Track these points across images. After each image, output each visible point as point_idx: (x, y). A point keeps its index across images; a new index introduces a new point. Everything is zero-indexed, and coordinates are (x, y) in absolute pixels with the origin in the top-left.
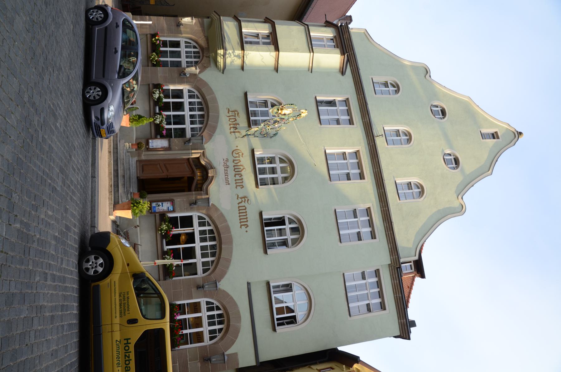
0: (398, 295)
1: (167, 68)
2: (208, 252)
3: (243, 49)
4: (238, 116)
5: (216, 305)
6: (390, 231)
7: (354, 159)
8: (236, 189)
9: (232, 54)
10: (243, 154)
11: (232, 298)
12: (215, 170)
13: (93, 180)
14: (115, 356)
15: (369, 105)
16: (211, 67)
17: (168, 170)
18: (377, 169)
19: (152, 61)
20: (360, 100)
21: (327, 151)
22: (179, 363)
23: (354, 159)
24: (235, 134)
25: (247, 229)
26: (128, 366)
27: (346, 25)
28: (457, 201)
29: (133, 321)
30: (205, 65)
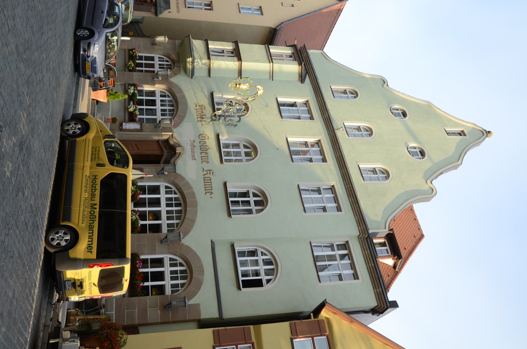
0: (370, 265)
1: (142, 73)
2: (174, 216)
3: (209, 58)
4: (205, 109)
5: (179, 262)
6: (356, 205)
7: (319, 155)
8: (203, 172)
9: (200, 62)
10: (208, 137)
11: (195, 253)
12: (183, 148)
13: (75, 109)
14: (84, 185)
15: (328, 106)
16: (181, 74)
17: (138, 149)
18: (339, 153)
19: (128, 67)
20: (319, 101)
21: (290, 139)
22: (138, 309)
23: (317, 148)
24: (202, 123)
25: (212, 196)
26: (94, 193)
27: (303, 46)
28: (426, 185)
29: (102, 165)
30: (176, 72)
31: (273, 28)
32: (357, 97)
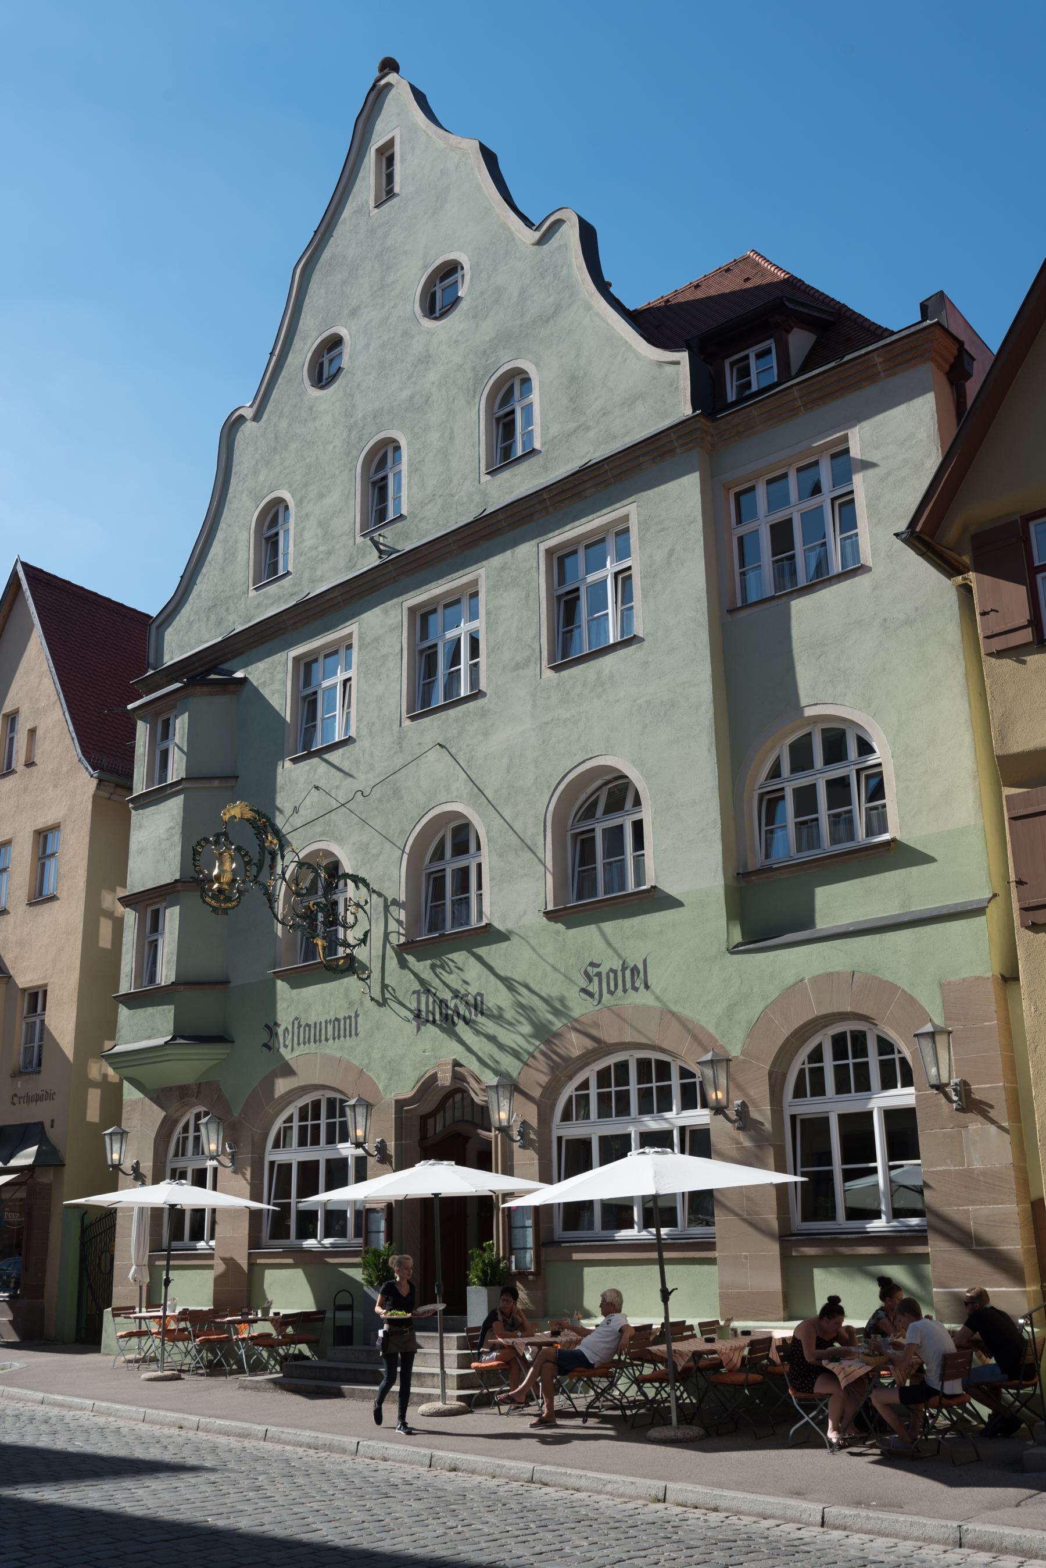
5: (806, 1062)
31: (100, 781)
32: (526, 372)
